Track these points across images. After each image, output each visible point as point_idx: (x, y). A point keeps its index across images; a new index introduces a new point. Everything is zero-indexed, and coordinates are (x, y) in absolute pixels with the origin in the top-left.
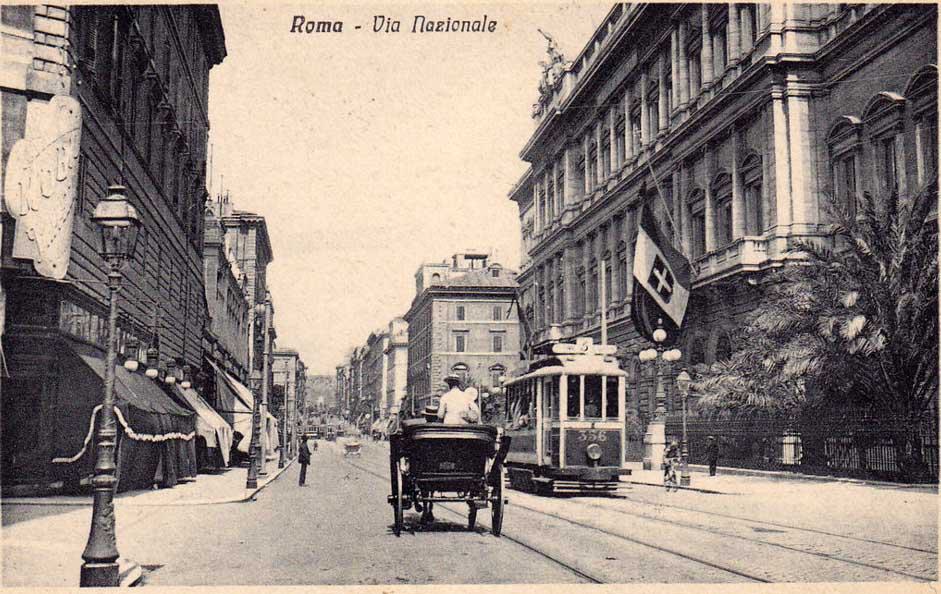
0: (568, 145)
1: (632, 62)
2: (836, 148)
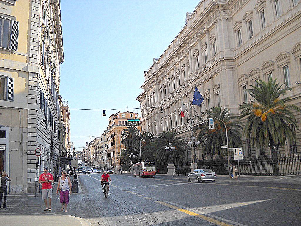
0: (156, 84)
1: (176, 60)
2: (240, 83)
